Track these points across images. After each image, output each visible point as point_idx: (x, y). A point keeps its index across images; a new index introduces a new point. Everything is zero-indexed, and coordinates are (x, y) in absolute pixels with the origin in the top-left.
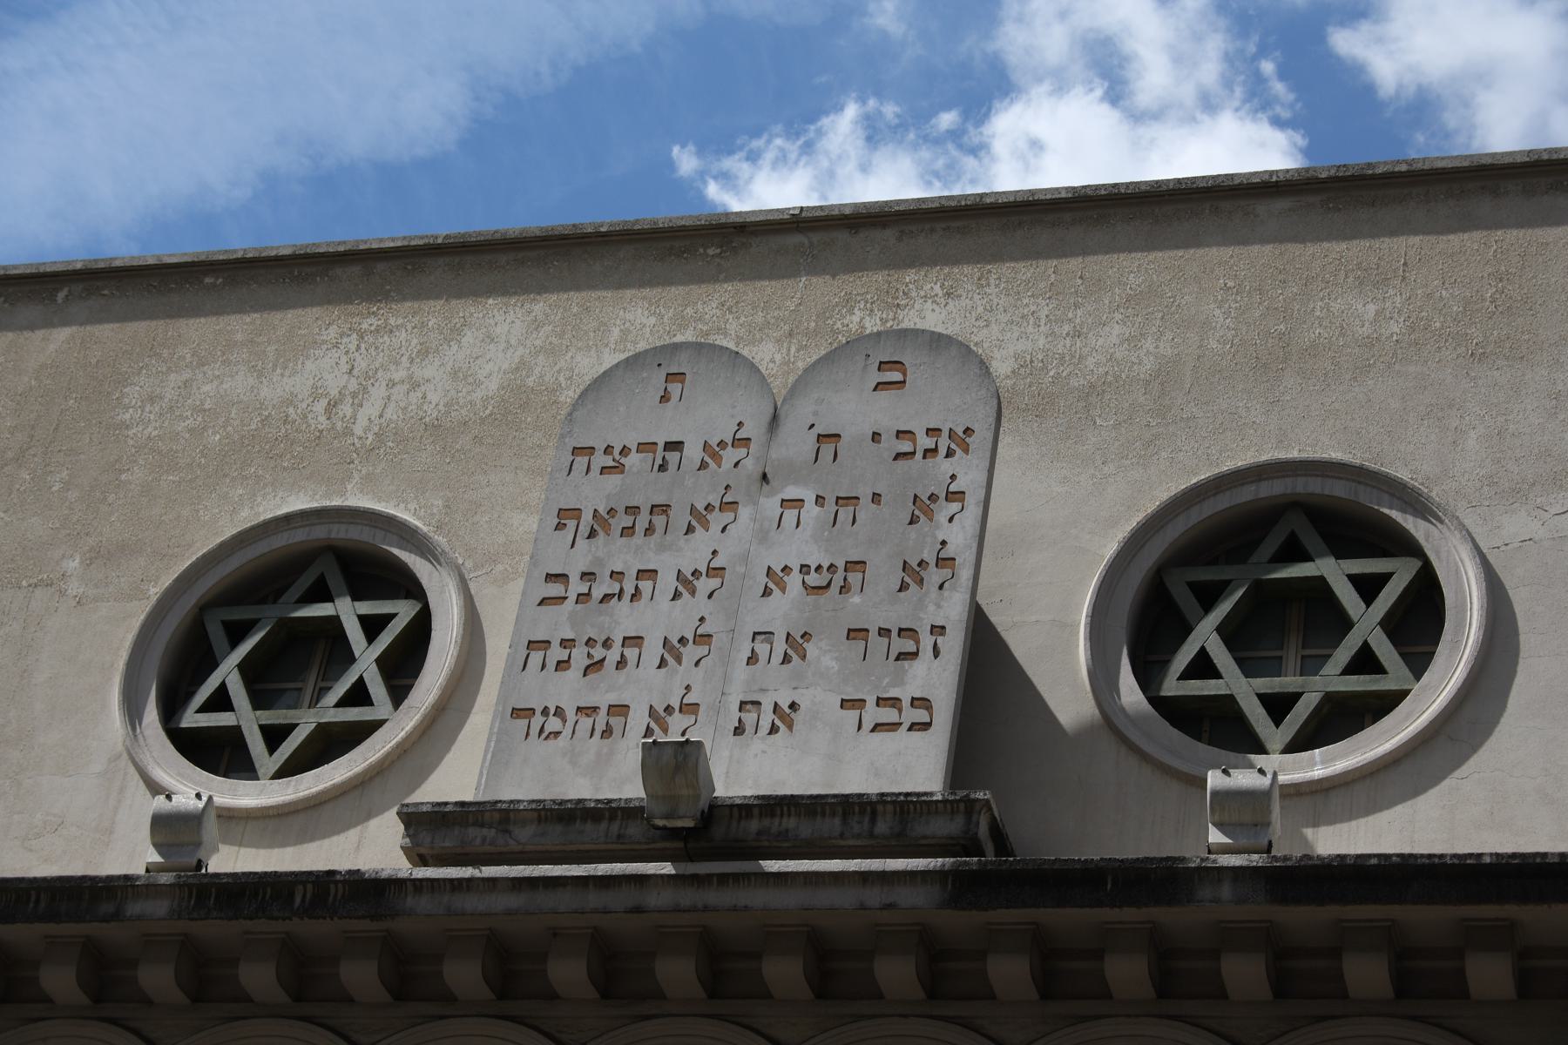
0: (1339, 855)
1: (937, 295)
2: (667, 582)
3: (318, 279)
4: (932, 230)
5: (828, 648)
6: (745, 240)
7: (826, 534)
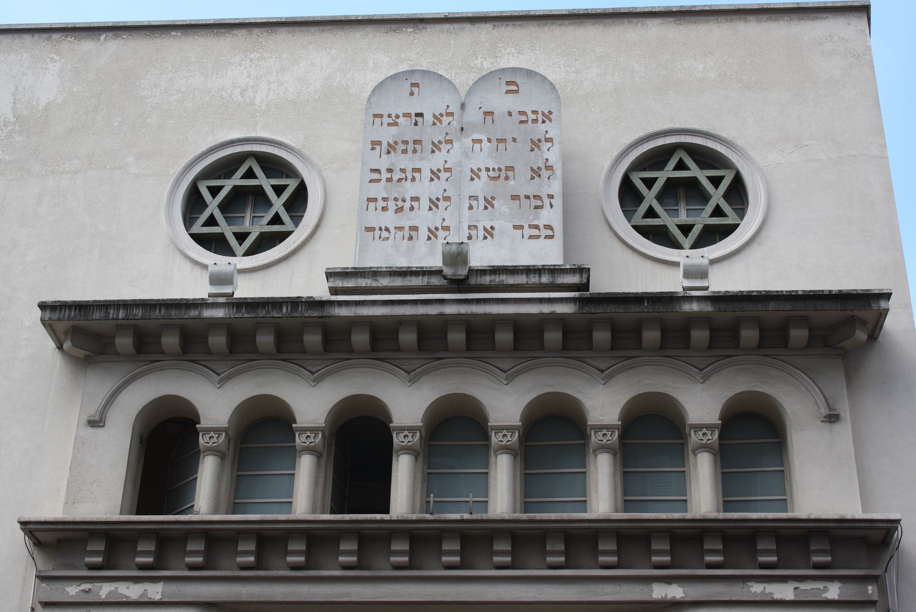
0: (740, 291)
1: (513, 53)
2: (426, 174)
3: (227, 35)
4: (508, 25)
5: (503, 203)
6: (424, 26)
7: (494, 154)
